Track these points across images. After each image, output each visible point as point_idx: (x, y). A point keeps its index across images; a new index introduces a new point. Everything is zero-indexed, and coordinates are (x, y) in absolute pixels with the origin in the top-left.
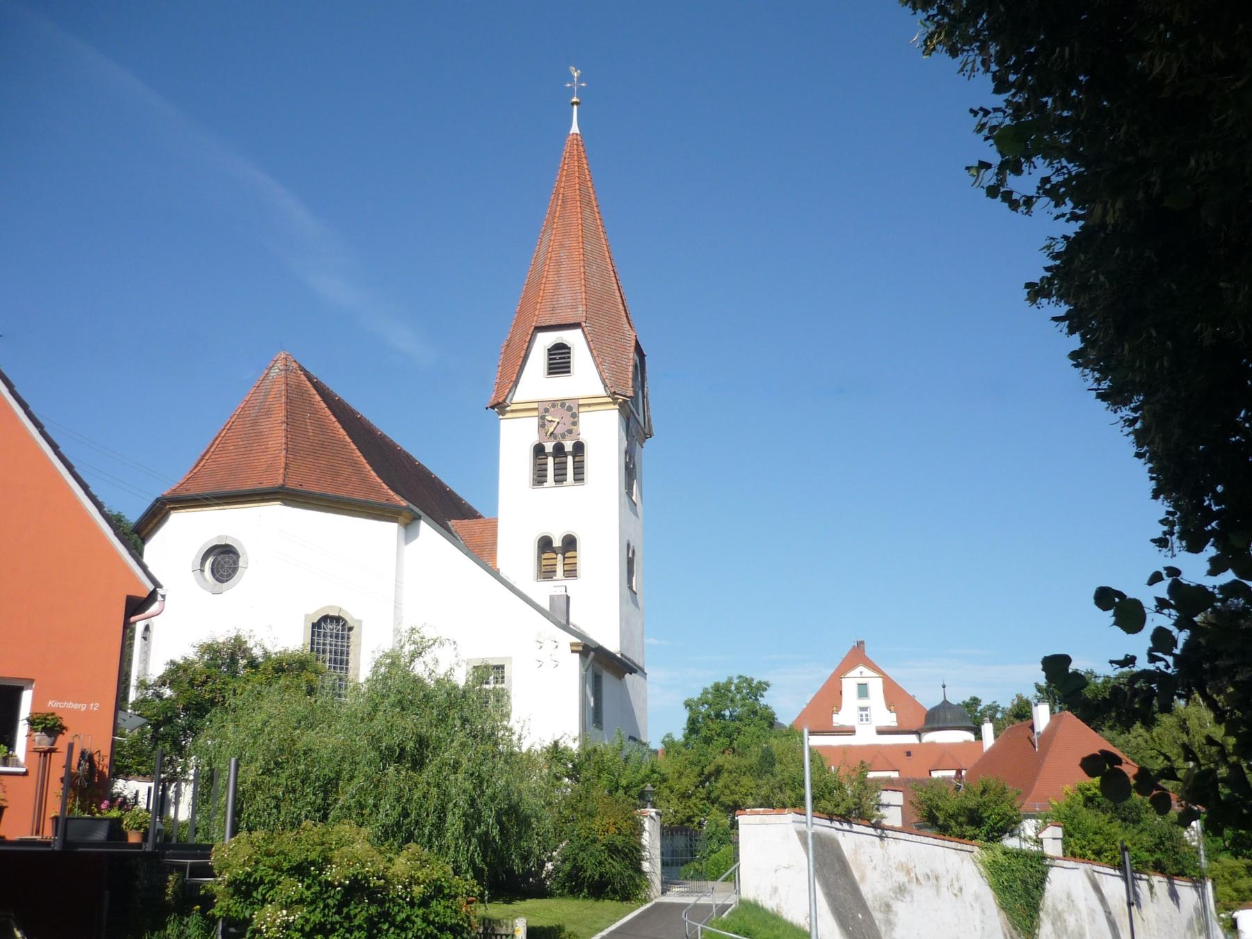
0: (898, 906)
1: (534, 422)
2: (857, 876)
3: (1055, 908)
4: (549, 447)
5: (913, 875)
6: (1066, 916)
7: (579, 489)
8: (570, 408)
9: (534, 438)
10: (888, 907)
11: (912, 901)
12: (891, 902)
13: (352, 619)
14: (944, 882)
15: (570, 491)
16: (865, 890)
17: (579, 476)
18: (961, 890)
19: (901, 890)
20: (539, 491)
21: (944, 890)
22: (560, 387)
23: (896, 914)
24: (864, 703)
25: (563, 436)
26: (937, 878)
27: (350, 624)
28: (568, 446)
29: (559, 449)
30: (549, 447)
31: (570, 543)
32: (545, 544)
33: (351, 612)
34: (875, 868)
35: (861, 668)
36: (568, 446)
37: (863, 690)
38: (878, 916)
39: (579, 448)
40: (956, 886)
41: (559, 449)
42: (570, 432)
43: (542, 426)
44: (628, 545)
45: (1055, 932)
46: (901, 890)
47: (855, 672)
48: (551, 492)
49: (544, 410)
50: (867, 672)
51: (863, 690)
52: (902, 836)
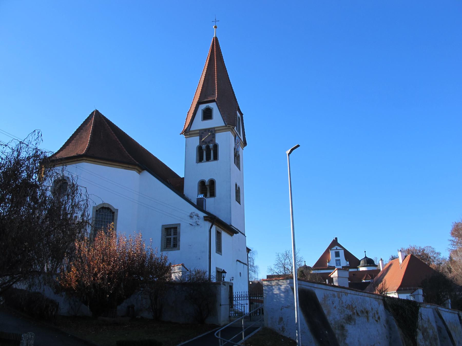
0: (350, 328)
1: (198, 138)
2: (325, 312)
3: (423, 327)
4: (204, 147)
5: (355, 311)
6: (428, 330)
7: (215, 162)
8: (212, 132)
9: (198, 144)
10: (342, 328)
11: (355, 324)
12: (344, 325)
13: (114, 208)
14: (371, 314)
15: (212, 164)
16: (330, 318)
17: (216, 158)
18: (379, 318)
19: (349, 319)
20: (200, 164)
21: (370, 318)
22: (208, 124)
23: (347, 331)
24: (338, 258)
25: (209, 142)
26: (367, 312)
27: (113, 211)
28: (211, 145)
29: (208, 147)
30: (204, 147)
31: (212, 182)
32: (202, 183)
33: (114, 205)
34: (335, 308)
35: (336, 247)
36: (211, 145)
37: (337, 254)
38: (337, 332)
39: (216, 146)
40: (377, 316)
41: (208, 147)
42: (212, 141)
43: (201, 139)
44: (236, 185)
45: (424, 338)
46: (349, 319)
47: (335, 248)
48: (206, 165)
49: (201, 133)
50: (339, 248)
51: (337, 254)
52: (349, 291)
